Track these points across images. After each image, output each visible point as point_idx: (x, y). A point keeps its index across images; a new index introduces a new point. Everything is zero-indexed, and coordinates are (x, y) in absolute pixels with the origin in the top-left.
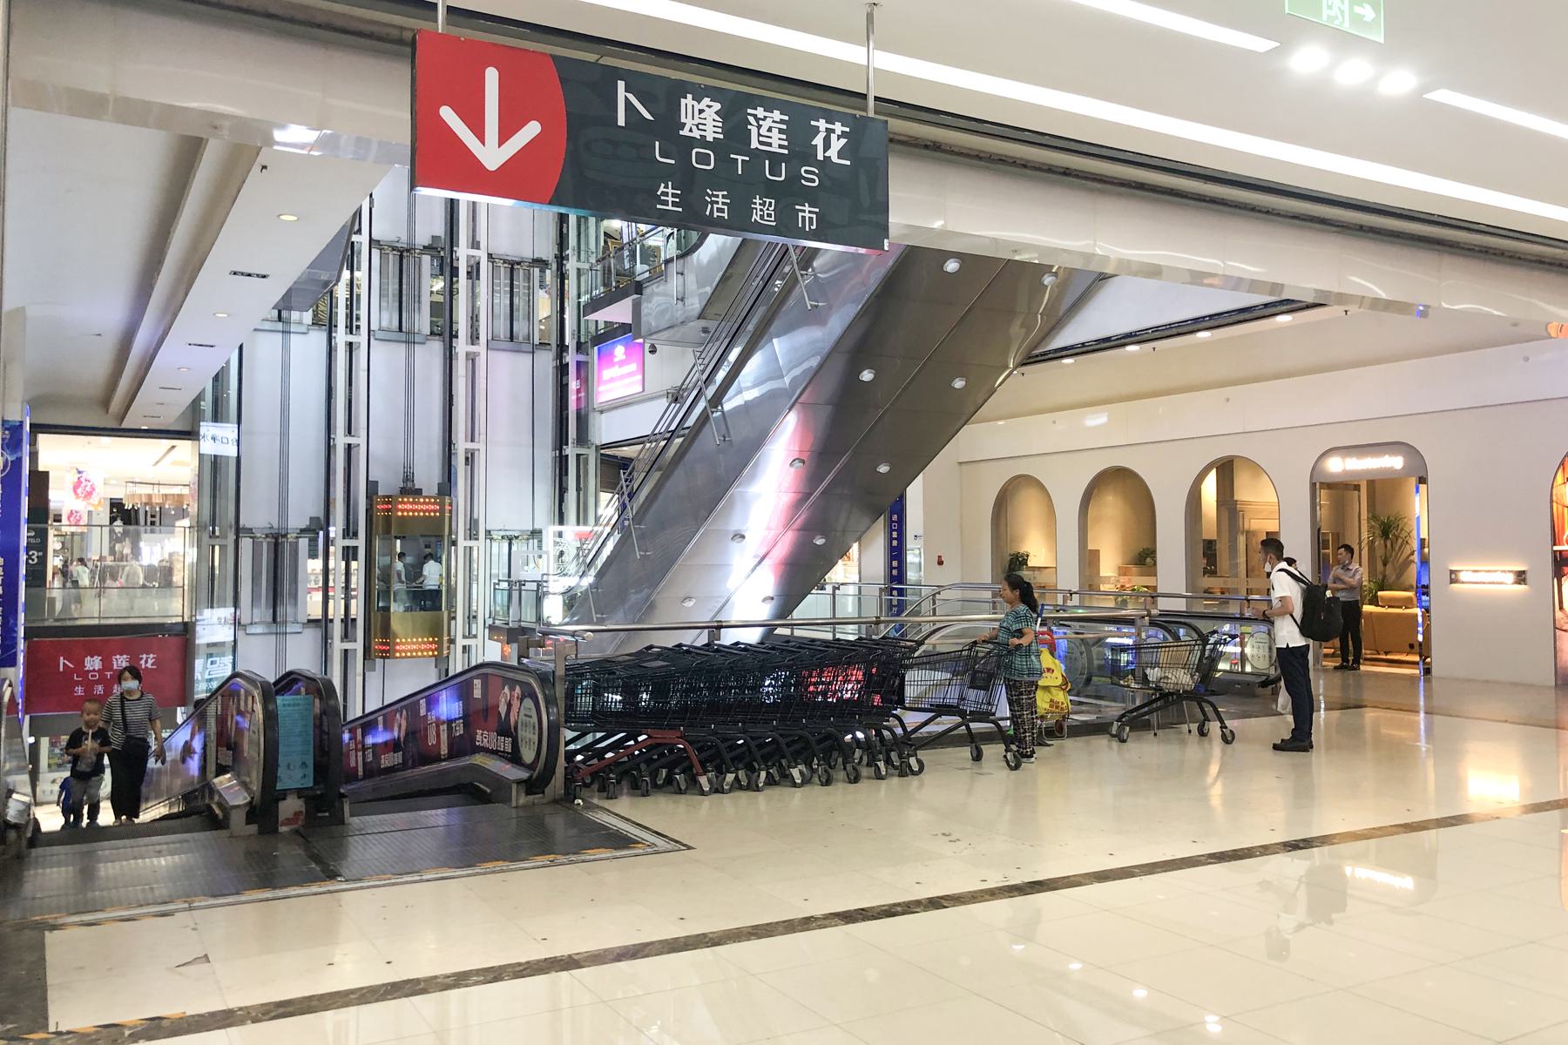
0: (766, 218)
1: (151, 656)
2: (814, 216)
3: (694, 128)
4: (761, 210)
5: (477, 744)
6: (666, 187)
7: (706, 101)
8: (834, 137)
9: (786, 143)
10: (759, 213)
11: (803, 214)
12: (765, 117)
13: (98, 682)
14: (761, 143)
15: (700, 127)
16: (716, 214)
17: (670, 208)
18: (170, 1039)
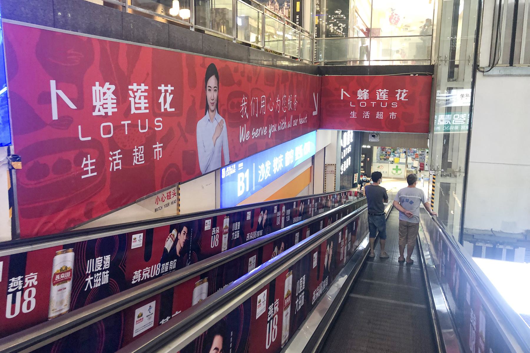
0: (380, 117)
1: (405, 91)
2: (395, 115)
3: (361, 97)
4: (379, 115)
5: (294, 218)
6: (353, 112)
7: (365, 90)
8: (403, 94)
9: (387, 97)
10: (378, 116)
11: (392, 115)
12: (382, 92)
13: (366, 109)
14: (380, 98)
15: (363, 97)
16: (366, 117)
17: (353, 117)
18: (69, 100)
